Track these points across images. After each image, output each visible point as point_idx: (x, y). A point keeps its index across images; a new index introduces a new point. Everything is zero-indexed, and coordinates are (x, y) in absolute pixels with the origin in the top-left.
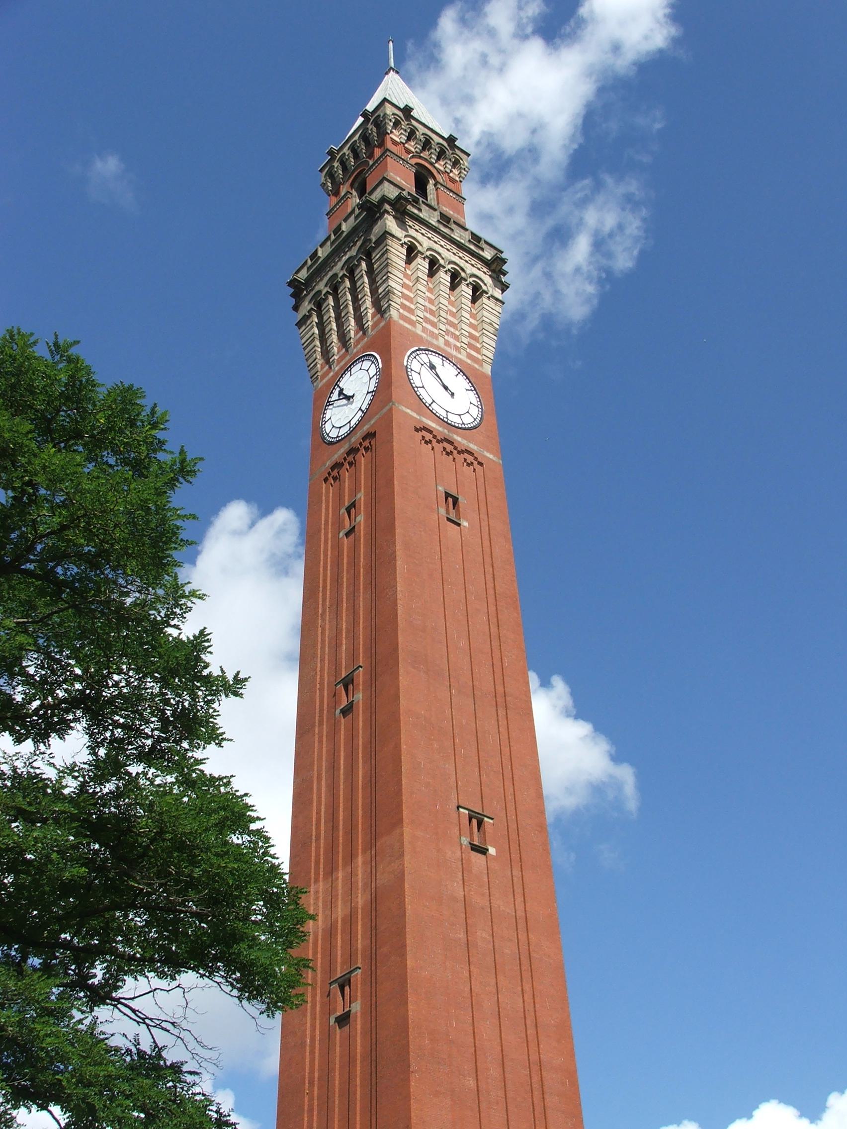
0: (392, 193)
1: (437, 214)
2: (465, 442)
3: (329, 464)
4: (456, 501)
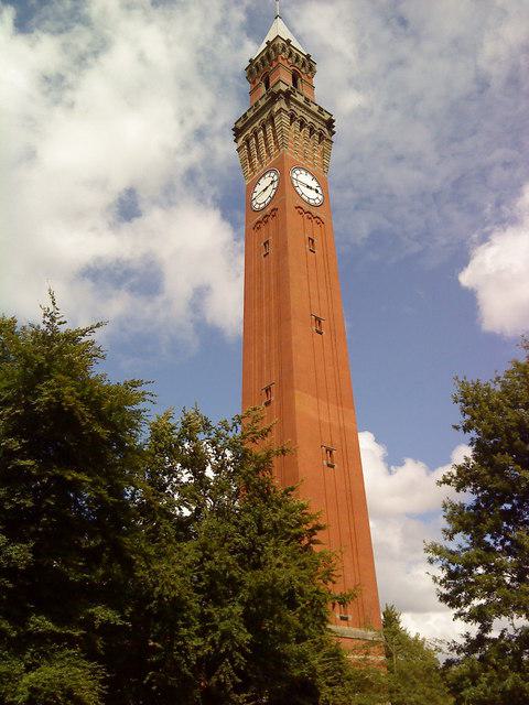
0: (284, 88)
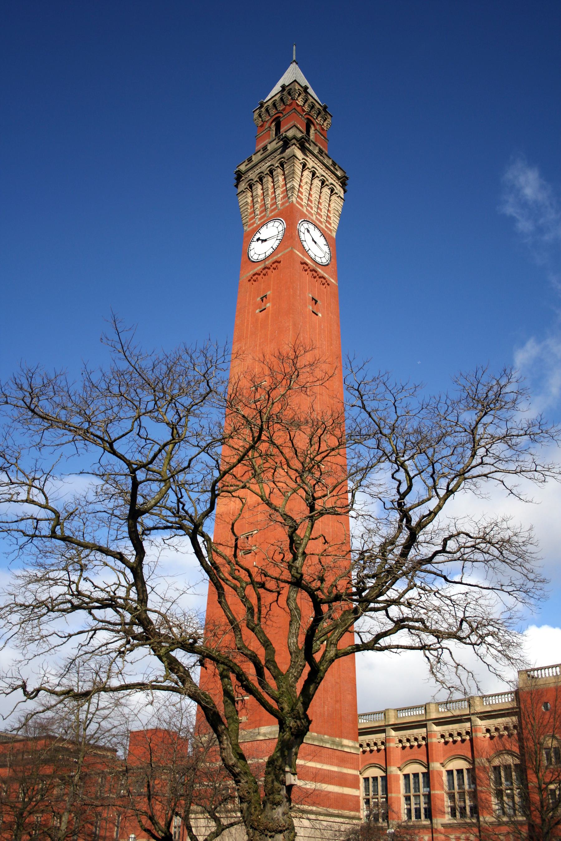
1: (317, 148)
2: (322, 272)
3: (252, 272)
4: (316, 302)
